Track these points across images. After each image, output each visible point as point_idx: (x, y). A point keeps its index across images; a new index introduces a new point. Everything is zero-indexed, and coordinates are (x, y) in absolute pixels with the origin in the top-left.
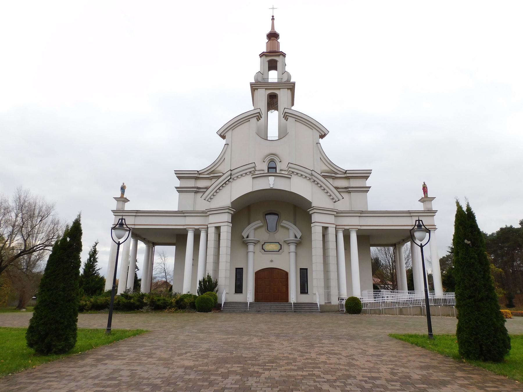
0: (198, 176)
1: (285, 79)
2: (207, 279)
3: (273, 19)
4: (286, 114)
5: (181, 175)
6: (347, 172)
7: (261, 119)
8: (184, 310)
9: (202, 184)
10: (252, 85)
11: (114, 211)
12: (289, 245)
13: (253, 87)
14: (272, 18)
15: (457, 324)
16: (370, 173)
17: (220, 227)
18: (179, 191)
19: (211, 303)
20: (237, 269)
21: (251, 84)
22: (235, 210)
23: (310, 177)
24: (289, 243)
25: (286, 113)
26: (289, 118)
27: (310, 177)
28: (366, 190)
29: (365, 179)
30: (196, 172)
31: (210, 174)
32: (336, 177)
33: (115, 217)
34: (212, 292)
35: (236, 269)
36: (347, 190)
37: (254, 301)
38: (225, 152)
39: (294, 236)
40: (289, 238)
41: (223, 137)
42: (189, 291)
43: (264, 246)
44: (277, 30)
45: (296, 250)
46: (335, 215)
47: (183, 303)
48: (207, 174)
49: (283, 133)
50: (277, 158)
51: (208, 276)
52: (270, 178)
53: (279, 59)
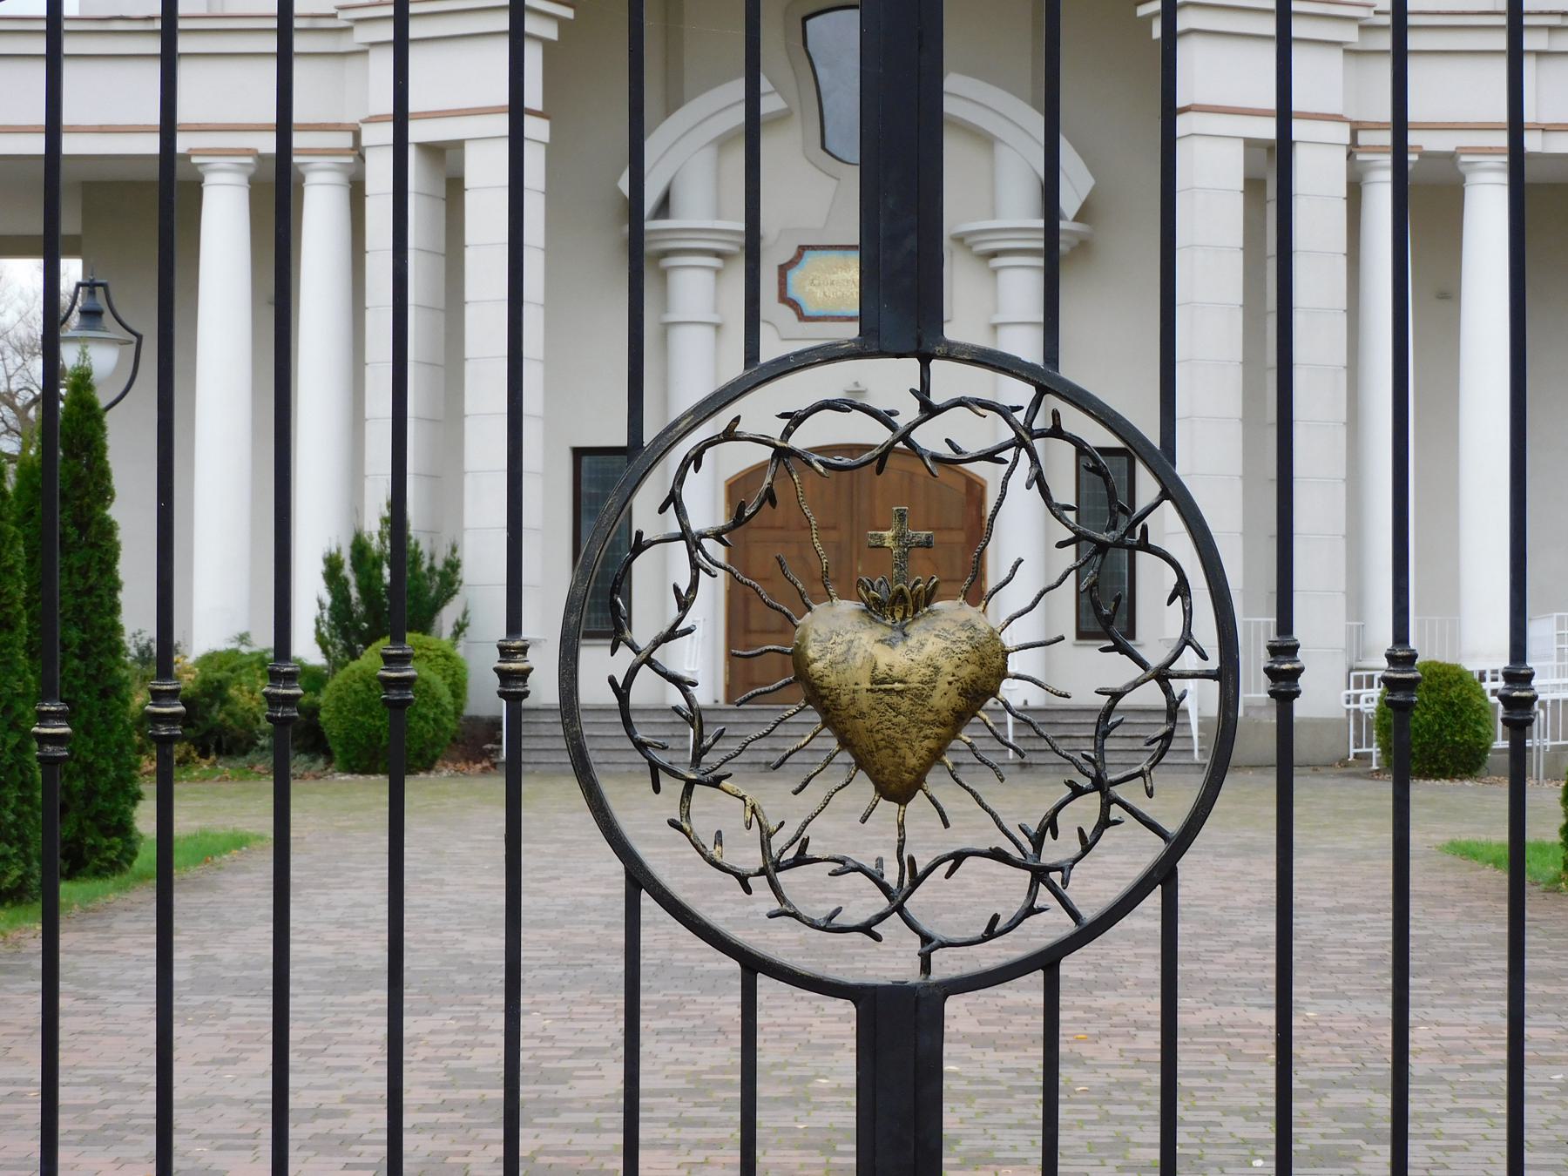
2: (383, 542)
8: (242, 762)
11: (613, 651)
12: (995, 271)
17: (459, 145)
19: (432, 715)
20: (585, 460)
22: (568, 13)
24: (995, 254)
34: (427, 638)
35: (579, 453)
37: (721, 698)
40: (994, 217)
42: (243, 630)
43: (794, 276)
46: (1346, 47)
47: (231, 715)
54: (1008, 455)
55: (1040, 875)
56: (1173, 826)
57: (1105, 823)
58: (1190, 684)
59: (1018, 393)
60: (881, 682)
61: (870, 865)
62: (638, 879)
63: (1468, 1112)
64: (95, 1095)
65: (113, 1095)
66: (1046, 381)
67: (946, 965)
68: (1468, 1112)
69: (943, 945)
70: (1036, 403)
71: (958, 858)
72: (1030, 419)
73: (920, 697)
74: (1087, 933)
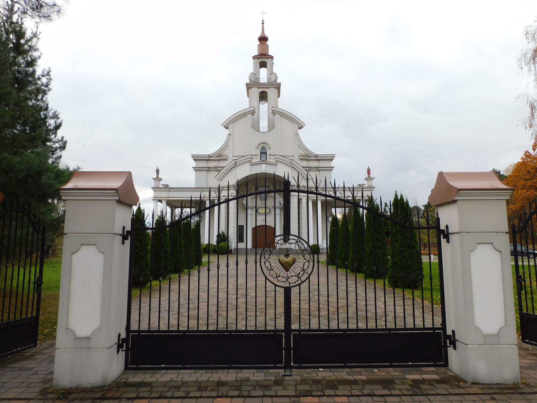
0: (209, 158)
1: (273, 80)
3: (263, 23)
4: (274, 111)
5: (196, 158)
6: (318, 156)
7: (255, 114)
9: (212, 164)
10: (247, 85)
13: (248, 87)
14: (262, 22)
15: (424, 270)
16: (334, 157)
18: (195, 170)
21: (247, 84)
23: (290, 164)
25: (273, 110)
26: (276, 115)
27: (290, 164)
28: (330, 169)
29: (331, 161)
30: (208, 156)
31: (217, 157)
32: (310, 159)
33: (154, 193)
36: (317, 169)
38: (229, 139)
39: (279, 203)
41: (227, 128)
44: (267, 34)
45: (280, 213)
48: (215, 157)
49: (271, 126)
50: (267, 146)
51: (222, 232)
52: (263, 165)
53: (268, 61)
54: (296, 243)
55: (299, 278)
56: (309, 273)
57: (304, 273)
58: (310, 262)
59: (296, 238)
60: (286, 262)
61: (285, 277)
62: (266, 278)
63: (323, 288)
64: (203, 287)
65: (204, 287)
66: (299, 237)
67: (291, 285)
68: (323, 288)
69: (291, 283)
70: (298, 239)
71: (292, 276)
72: (297, 240)
73: (289, 263)
74: (303, 282)
